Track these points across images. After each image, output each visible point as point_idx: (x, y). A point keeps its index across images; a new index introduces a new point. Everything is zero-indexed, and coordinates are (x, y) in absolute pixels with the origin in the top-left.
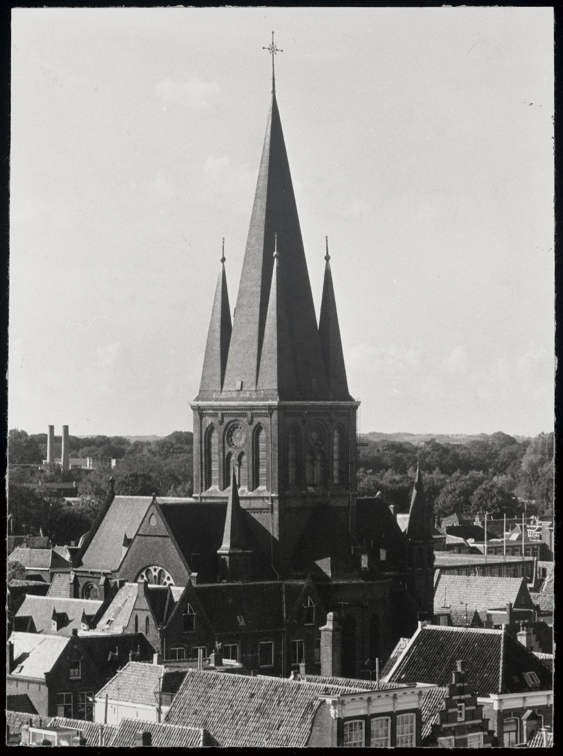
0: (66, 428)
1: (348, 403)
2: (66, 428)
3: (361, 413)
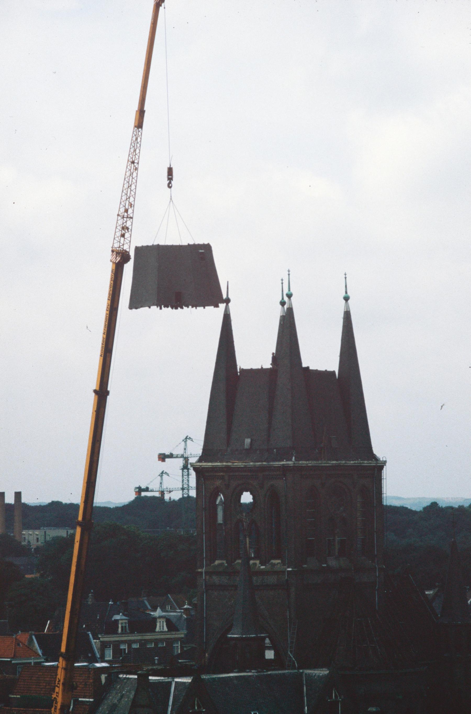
0: (18, 495)
1: (373, 463)
2: (18, 495)
3: (387, 473)
